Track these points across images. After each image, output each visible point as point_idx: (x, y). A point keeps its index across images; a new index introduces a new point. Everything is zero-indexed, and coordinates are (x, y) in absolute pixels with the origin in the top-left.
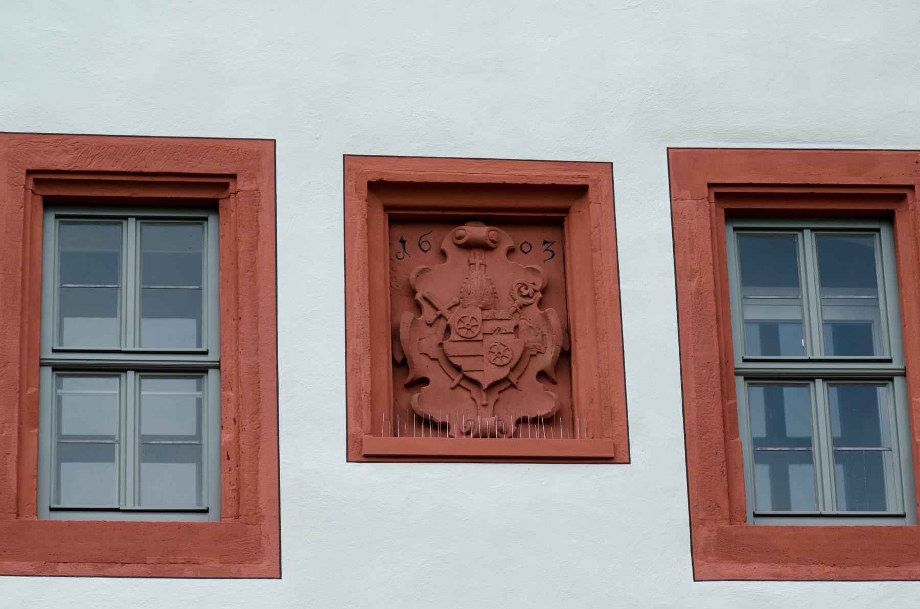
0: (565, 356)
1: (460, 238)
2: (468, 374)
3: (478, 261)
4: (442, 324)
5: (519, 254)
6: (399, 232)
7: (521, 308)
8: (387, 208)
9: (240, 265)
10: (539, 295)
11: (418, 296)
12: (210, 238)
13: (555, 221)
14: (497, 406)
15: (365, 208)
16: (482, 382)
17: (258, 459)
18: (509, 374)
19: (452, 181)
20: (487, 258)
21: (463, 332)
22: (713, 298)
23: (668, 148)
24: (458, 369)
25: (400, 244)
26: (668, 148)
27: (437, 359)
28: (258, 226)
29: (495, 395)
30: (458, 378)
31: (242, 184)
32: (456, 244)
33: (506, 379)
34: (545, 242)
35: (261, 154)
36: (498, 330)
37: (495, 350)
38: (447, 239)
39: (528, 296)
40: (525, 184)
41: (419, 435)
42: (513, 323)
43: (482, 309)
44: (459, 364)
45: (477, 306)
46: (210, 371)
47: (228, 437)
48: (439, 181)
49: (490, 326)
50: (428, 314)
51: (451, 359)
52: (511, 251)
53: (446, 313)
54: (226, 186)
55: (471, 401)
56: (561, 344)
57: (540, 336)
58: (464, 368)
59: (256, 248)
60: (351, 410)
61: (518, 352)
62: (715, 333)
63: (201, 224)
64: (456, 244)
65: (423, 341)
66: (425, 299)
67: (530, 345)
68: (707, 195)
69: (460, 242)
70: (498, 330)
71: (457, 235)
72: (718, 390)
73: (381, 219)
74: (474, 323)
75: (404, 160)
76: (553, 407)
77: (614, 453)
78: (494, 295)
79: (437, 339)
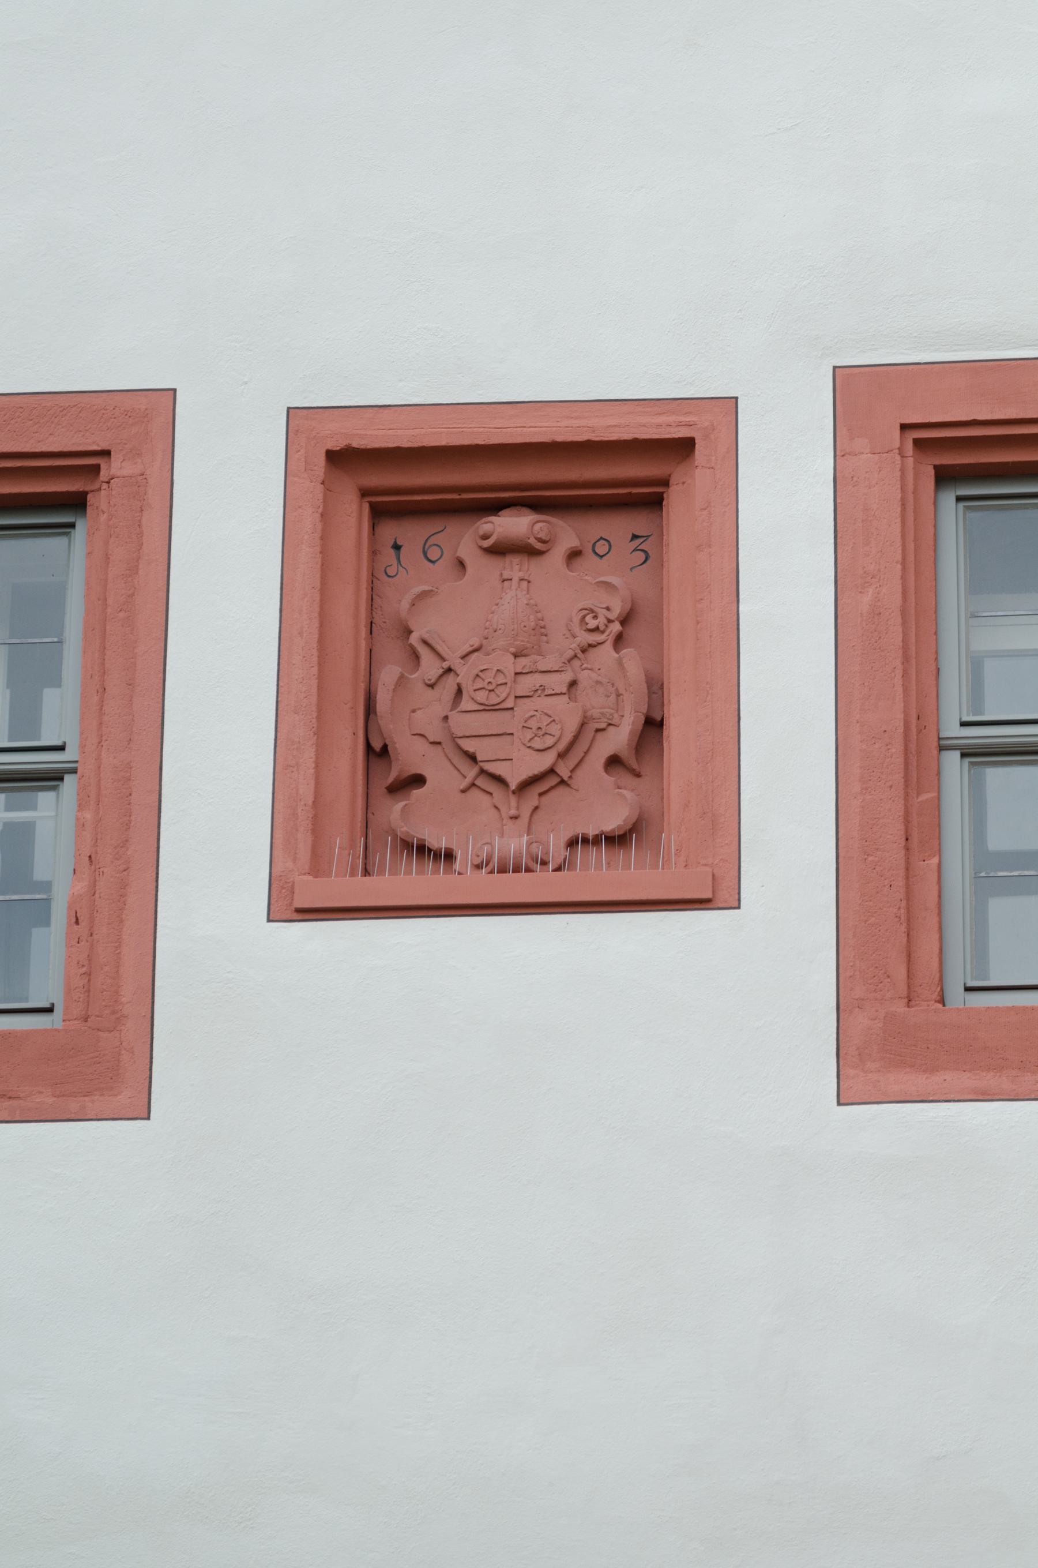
0: (653, 726)
1: (485, 537)
2: (487, 767)
3: (516, 575)
4: (450, 682)
5: (589, 561)
6: (390, 531)
7: (584, 651)
8: (365, 493)
9: (110, 601)
10: (616, 627)
11: (414, 639)
12: (64, 562)
13: (650, 500)
14: (535, 817)
15: (320, 496)
16: (509, 780)
17: (122, 921)
18: (554, 764)
19: (466, 442)
20: (535, 568)
21: (481, 696)
22: (899, 620)
23: (835, 368)
24: (472, 758)
25: (392, 551)
26: (835, 368)
27: (440, 743)
28: (141, 535)
29: (532, 798)
30: (471, 773)
31: (116, 467)
32: (480, 547)
33: (551, 771)
34: (635, 537)
35: (149, 415)
36: (540, 691)
37: (533, 724)
38: (464, 538)
39: (596, 629)
40: (588, 441)
41: (421, 872)
42: (567, 677)
43: (516, 656)
44: (471, 750)
45: (507, 651)
46: (67, 777)
47: (82, 887)
48: (443, 443)
49: (526, 684)
50: (430, 667)
51: (460, 742)
52: (574, 555)
53: (456, 664)
54: (97, 469)
55: (494, 810)
56: (644, 709)
57: (613, 697)
58: (479, 758)
59: (137, 573)
60: (279, 834)
61: (572, 726)
62: (898, 681)
63: (67, 534)
64: (480, 547)
65: (418, 712)
66: (425, 643)
67: (595, 713)
68: (898, 445)
69: (486, 544)
70: (540, 691)
71: (481, 533)
72: (898, 778)
73: (352, 513)
74: (501, 679)
75: (387, 411)
76: (616, 812)
77: (714, 894)
78: (540, 630)
79: (440, 708)
